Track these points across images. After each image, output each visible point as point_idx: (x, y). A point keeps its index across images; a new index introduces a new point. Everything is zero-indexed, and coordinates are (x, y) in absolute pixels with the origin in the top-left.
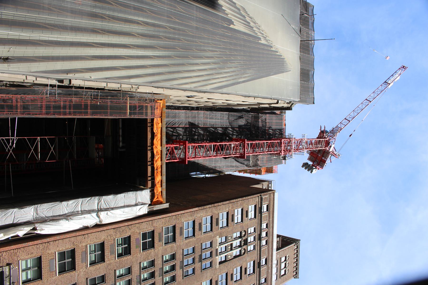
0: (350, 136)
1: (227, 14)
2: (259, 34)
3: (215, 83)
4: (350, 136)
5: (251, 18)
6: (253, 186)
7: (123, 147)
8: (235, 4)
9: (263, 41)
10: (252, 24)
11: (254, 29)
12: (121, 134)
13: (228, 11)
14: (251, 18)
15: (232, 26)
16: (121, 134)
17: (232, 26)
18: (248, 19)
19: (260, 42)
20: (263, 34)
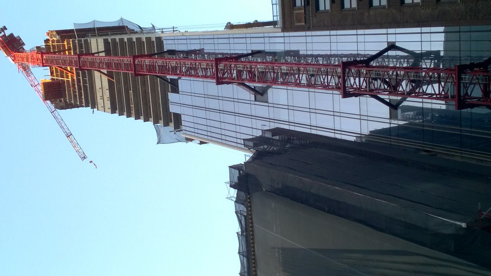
3: (404, 263)
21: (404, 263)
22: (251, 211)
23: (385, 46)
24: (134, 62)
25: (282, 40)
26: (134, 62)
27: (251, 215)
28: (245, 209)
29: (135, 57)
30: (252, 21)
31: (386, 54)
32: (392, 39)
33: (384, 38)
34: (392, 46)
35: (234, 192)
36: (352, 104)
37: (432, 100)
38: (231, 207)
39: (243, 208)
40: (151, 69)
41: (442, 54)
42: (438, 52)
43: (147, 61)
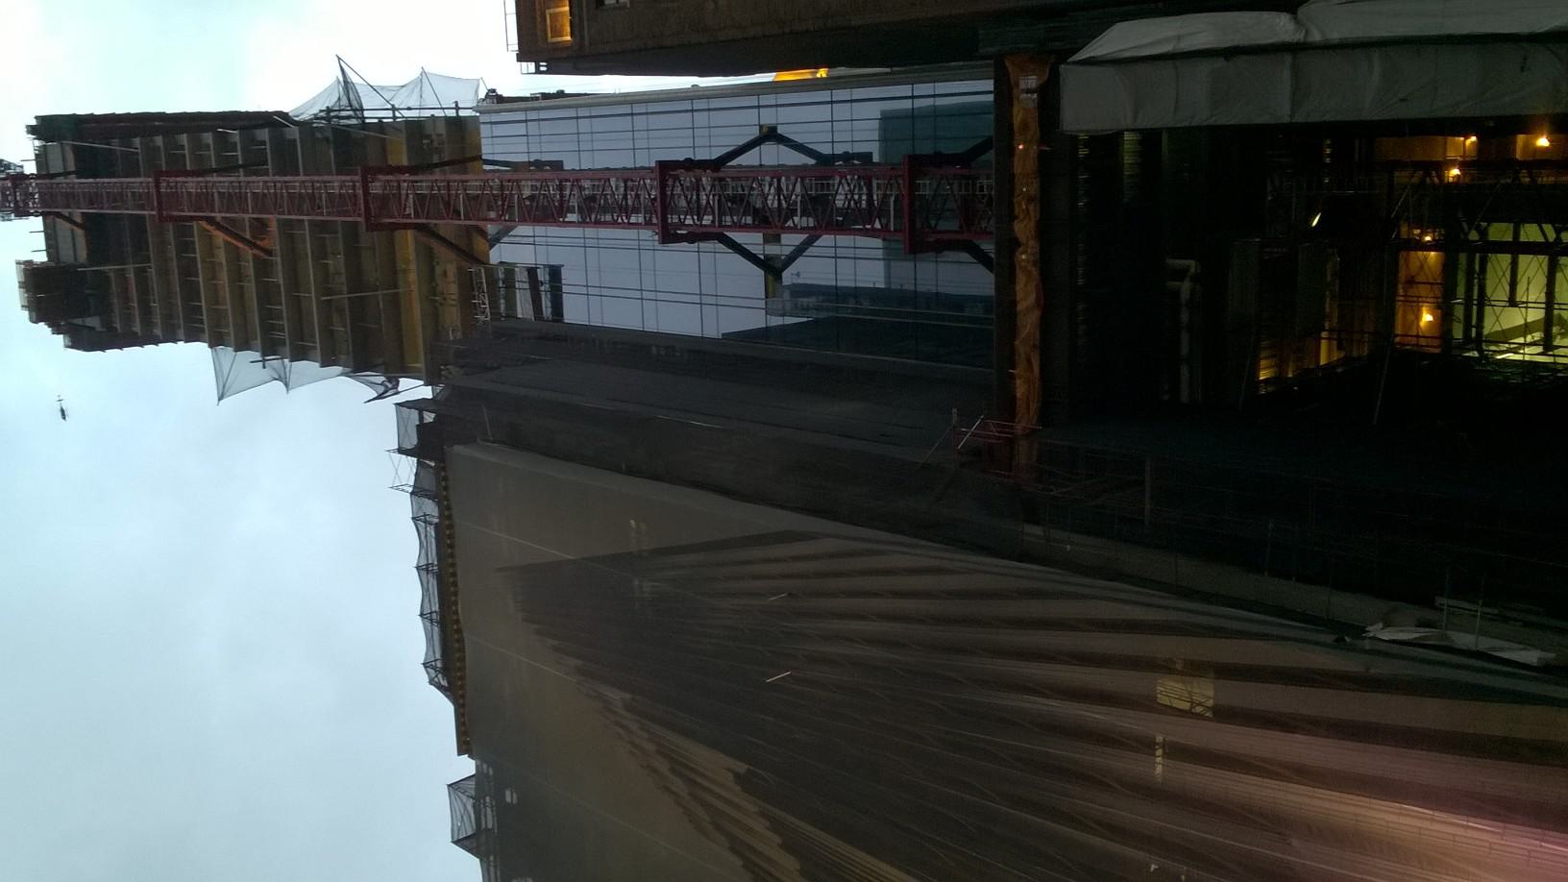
0: (63, 411)
1: (763, 815)
2: (634, 727)
3: (796, 559)
4: (63, 411)
5: (667, 789)
6: (1128, 159)
7: (1180, 275)
8: (733, 850)
9: (616, 696)
10: (663, 766)
11: (651, 747)
12: (1185, 337)
13: (759, 825)
14: (667, 789)
15: (742, 767)
16: (1185, 337)
17: (742, 767)
18: (679, 785)
19: (628, 696)
20: (617, 724)
21: (796, 559)
22: (449, 508)
23: (755, 132)
24: (157, 186)
25: (521, 129)
26: (157, 186)
27: (449, 517)
28: (436, 513)
29: (158, 174)
30: (553, 91)
31: (733, 163)
32: (768, 118)
33: (751, 117)
34: (770, 135)
35: (408, 466)
36: (681, 259)
37: (852, 263)
38: (404, 506)
39: (431, 508)
40: (203, 201)
41: (876, 159)
42: (866, 157)
43: (192, 184)
